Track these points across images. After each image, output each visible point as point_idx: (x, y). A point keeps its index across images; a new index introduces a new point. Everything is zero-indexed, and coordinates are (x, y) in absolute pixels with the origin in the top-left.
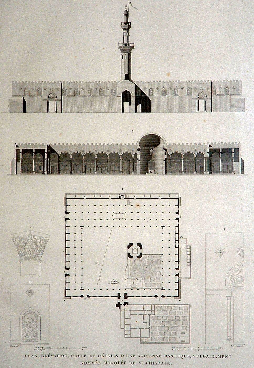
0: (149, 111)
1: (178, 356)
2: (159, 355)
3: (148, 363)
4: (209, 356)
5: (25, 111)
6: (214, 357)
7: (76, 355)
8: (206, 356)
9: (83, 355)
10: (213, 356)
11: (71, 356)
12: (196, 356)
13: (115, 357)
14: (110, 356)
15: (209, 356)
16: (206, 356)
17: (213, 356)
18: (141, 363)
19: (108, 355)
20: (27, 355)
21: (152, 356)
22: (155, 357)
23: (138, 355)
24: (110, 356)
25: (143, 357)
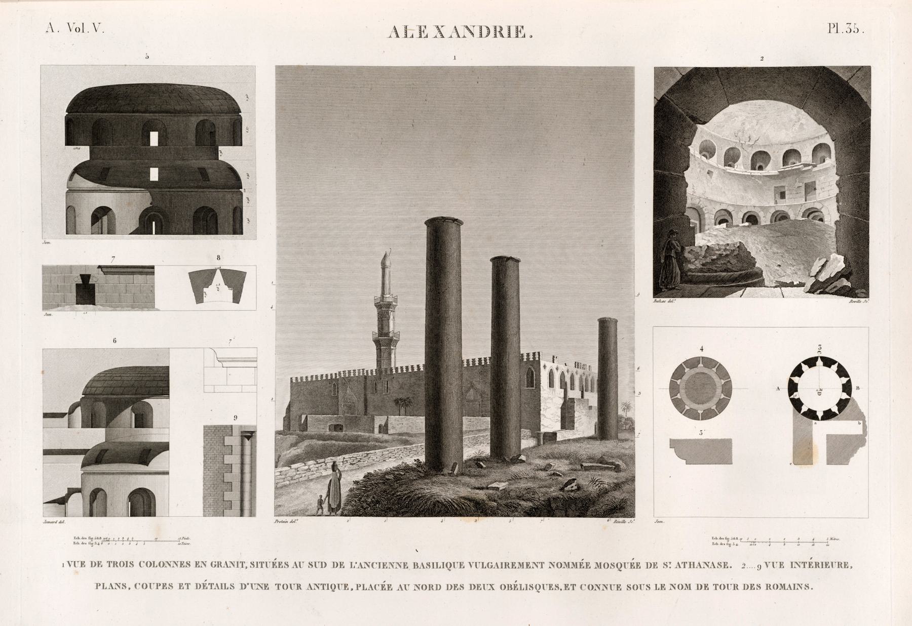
0: (44, 454)
1: (440, 564)
2: (570, 567)
3: (682, 566)
4: (499, 565)
5: (167, 473)
6: (843, 565)
7: (149, 566)
8: (494, 564)
9: (160, 585)
10: (507, 565)
11: (138, 564)
12: (474, 564)
13: (756, 589)
14: (500, 566)
15: (499, 565)
16: (494, 564)
17: (507, 565)
18: (668, 564)
19: (215, 584)
20: (100, 585)
21: (531, 565)
22: (395, 567)
23: (399, 586)
24: (500, 566)
25: (675, 588)
